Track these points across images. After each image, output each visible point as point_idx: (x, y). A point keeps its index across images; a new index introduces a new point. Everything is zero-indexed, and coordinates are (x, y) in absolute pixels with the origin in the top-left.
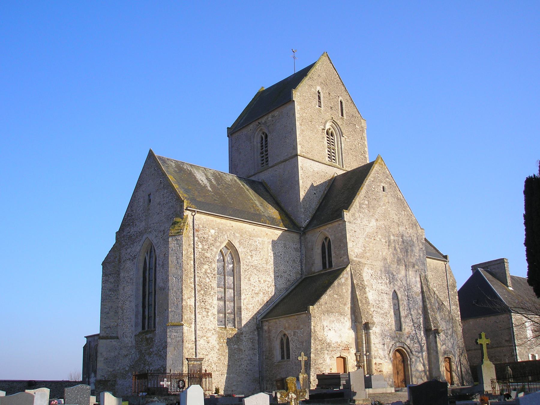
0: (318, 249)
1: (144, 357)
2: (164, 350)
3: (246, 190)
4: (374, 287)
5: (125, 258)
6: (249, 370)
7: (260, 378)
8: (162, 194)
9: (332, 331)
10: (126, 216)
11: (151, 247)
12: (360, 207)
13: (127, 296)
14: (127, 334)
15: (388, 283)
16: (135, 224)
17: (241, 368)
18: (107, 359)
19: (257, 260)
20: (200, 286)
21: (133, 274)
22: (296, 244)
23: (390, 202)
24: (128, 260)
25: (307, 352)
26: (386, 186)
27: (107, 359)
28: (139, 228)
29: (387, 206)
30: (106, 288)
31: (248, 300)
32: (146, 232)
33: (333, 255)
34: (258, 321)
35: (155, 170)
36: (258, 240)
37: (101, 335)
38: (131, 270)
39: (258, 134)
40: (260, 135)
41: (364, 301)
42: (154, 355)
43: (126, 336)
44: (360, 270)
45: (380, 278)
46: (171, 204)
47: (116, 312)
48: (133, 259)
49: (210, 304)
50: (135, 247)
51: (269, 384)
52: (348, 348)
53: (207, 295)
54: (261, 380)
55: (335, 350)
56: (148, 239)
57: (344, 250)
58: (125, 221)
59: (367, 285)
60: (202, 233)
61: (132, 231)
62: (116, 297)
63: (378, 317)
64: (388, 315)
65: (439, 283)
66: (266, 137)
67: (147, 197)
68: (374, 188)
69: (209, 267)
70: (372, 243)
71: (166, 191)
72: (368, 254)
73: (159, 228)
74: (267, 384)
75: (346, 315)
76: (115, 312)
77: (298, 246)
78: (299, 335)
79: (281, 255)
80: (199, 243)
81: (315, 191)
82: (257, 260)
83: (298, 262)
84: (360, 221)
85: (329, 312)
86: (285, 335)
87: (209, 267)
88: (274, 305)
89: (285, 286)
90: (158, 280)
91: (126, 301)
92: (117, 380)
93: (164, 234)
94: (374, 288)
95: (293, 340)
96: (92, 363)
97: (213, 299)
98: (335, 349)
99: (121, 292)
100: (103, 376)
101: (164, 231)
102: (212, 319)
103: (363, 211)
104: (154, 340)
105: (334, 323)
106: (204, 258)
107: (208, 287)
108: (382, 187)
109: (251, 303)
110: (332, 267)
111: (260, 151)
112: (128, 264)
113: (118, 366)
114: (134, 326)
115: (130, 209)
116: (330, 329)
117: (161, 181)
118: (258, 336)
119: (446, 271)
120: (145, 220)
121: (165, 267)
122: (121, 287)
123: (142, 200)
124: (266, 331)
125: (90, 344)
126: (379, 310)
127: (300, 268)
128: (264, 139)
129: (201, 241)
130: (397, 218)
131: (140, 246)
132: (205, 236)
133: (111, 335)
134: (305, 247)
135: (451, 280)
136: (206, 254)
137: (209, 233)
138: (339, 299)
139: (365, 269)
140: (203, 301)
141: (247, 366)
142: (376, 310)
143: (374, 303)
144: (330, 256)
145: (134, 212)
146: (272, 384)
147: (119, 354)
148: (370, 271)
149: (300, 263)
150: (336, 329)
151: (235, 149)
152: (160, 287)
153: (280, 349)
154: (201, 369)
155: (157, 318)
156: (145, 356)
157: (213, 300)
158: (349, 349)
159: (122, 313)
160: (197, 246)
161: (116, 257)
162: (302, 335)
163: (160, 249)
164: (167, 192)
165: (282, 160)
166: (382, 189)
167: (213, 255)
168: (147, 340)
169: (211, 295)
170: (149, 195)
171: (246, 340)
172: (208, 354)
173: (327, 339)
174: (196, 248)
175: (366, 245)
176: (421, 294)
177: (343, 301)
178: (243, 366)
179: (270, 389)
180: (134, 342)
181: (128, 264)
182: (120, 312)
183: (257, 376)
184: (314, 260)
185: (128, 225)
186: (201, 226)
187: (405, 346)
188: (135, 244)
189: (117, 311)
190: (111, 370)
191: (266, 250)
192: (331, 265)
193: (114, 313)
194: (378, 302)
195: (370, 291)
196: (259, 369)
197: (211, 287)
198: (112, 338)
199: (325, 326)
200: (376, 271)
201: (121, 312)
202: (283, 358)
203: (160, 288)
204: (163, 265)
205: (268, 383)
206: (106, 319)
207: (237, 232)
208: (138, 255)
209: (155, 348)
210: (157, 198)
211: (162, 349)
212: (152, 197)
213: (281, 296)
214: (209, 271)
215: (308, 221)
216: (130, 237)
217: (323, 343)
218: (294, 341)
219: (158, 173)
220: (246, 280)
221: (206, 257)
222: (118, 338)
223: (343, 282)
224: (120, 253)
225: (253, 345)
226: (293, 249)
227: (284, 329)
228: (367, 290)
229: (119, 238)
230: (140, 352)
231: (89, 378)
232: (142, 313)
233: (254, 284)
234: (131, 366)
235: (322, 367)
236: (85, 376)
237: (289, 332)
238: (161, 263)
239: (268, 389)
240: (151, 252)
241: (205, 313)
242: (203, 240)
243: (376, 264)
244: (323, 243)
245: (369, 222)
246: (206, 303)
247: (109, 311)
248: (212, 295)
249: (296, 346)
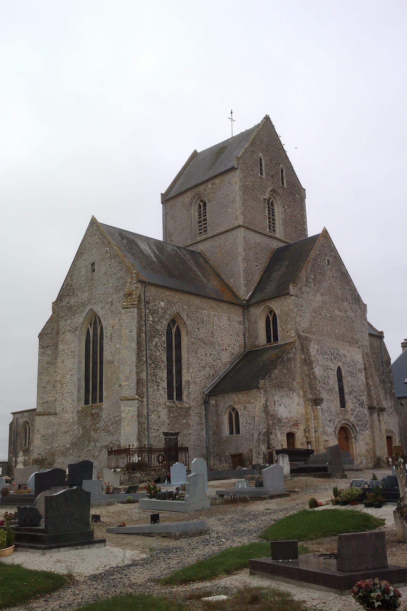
0: (262, 322)
1: (89, 433)
2: (112, 426)
3: (187, 261)
4: (320, 362)
5: (64, 330)
6: (197, 446)
7: (207, 454)
8: (108, 264)
9: (283, 406)
10: (64, 285)
11: (96, 318)
12: (306, 281)
13: (68, 370)
14: (68, 409)
15: (333, 358)
16: (76, 294)
17: (189, 444)
18: (44, 436)
19: (203, 333)
20: (151, 359)
21: (75, 347)
22: (239, 317)
23: (335, 276)
24: (67, 331)
25: (259, 427)
26: (331, 260)
27: (44, 436)
28: (80, 298)
29: (331, 280)
30: (43, 361)
31: (196, 373)
32: (89, 303)
33: (279, 329)
34: (205, 395)
35: (99, 238)
36: (205, 313)
37: (38, 410)
38: (72, 342)
39: (195, 203)
40: (198, 202)
41: (312, 377)
42: (101, 431)
43: (66, 411)
44: (307, 344)
45: (326, 353)
46: (119, 275)
47: (54, 387)
48: (75, 331)
49: (160, 377)
50: (76, 318)
51: (217, 460)
52: (298, 424)
53: (157, 369)
54: (208, 456)
55: (285, 426)
56: (93, 310)
57: (291, 325)
58: (64, 290)
59: (313, 361)
60: (152, 305)
61: (73, 301)
62: (54, 370)
63: (324, 392)
64: (334, 392)
65: (374, 360)
66: (205, 205)
67: (90, 267)
68: (320, 262)
69: (159, 340)
70: (318, 317)
71: (113, 261)
72: (314, 329)
73: (106, 300)
74: (214, 460)
75: (294, 390)
76: (53, 386)
77: (241, 319)
78: (250, 410)
79: (225, 328)
80: (150, 316)
81: (257, 263)
82: (203, 333)
83: (241, 336)
84: (307, 296)
85: (279, 386)
86: (234, 409)
87: (160, 340)
88: (220, 379)
89: (230, 360)
90: (105, 354)
91: (66, 375)
92: (55, 459)
93: (112, 305)
94: (320, 363)
95: (244, 415)
96: (20, 441)
97: (163, 373)
98: (285, 424)
99: (60, 364)
100: (39, 454)
101: (111, 302)
102: (163, 393)
103: (310, 285)
104: (100, 415)
105: (284, 398)
106: (154, 330)
107: (158, 361)
108: (327, 260)
109: (198, 376)
110: (278, 341)
111: (197, 220)
112: (69, 336)
113: (56, 444)
114: (76, 401)
115: (69, 278)
116: (280, 404)
117: (106, 250)
118: (205, 410)
119: (381, 348)
120: (89, 290)
121: (114, 340)
122: (59, 360)
123: (84, 270)
124: (213, 406)
125: (17, 421)
126: (325, 386)
127: (243, 341)
128: (202, 207)
129: (152, 313)
130: (341, 293)
131: (83, 317)
132: (155, 308)
133: (48, 411)
134: (248, 320)
135: (386, 357)
136: (156, 326)
137: (159, 305)
138: (288, 374)
139: (312, 345)
140: (154, 375)
141: (195, 442)
142: (322, 386)
143: (320, 379)
144: (275, 330)
145: (75, 281)
146: (220, 460)
147: (57, 430)
148: (316, 346)
149: (243, 336)
150: (286, 404)
151: (169, 217)
152: (108, 360)
153: (228, 424)
154: (176, 444)
155: (104, 392)
156: (90, 432)
157: (163, 374)
158: (299, 424)
159: (61, 388)
160: (148, 319)
161: (54, 328)
162: (253, 410)
163: (107, 321)
164: (114, 262)
165: (223, 230)
166: (327, 263)
167: (163, 328)
168: (92, 415)
169: (162, 368)
170: (93, 264)
171: (194, 415)
172: (159, 429)
173: (278, 414)
174: (147, 320)
175: (312, 320)
176: (364, 370)
177: (292, 376)
178: (191, 442)
179: (218, 465)
180: (76, 418)
181: (69, 336)
182: (59, 385)
183: (205, 451)
184: (258, 333)
185: (67, 295)
186: (151, 298)
187: (350, 423)
188: (77, 315)
189: (55, 385)
190: (49, 447)
191: (211, 322)
192: (276, 339)
193: (52, 387)
194: (324, 378)
195: (317, 366)
196: (206, 444)
197: (161, 360)
198: (49, 414)
199: (276, 401)
200: (321, 346)
201: (61, 386)
202: (231, 432)
203: (107, 361)
204: (111, 338)
205: (216, 459)
206: (43, 393)
207: (185, 304)
208: (80, 327)
209: (102, 424)
210: (102, 268)
211: (111, 425)
212: (96, 267)
213: (226, 369)
214: (159, 344)
215: (250, 293)
216: (70, 308)
217: (275, 419)
218: (244, 416)
219: (103, 242)
220: (193, 354)
221: (156, 330)
222: (56, 414)
223: (291, 357)
224: (58, 324)
225: (201, 420)
226: (237, 322)
227: (234, 403)
228: (314, 365)
229: (56, 308)
230: (84, 428)
231: (16, 457)
232: (84, 386)
233: (201, 357)
234: (72, 443)
235: (274, 443)
236: (11, 455)
237: (239, 406)
238: (108, 335)
239: (216, 465)
240: (95, 323)
241: (156, 387)
242: (153, 312)
243: (321, 339)
244: (268, 316)
245: (315, 296)
246: (157, 377)
247: (47, 385)
248: (162, 369)
249: (247, 421)
